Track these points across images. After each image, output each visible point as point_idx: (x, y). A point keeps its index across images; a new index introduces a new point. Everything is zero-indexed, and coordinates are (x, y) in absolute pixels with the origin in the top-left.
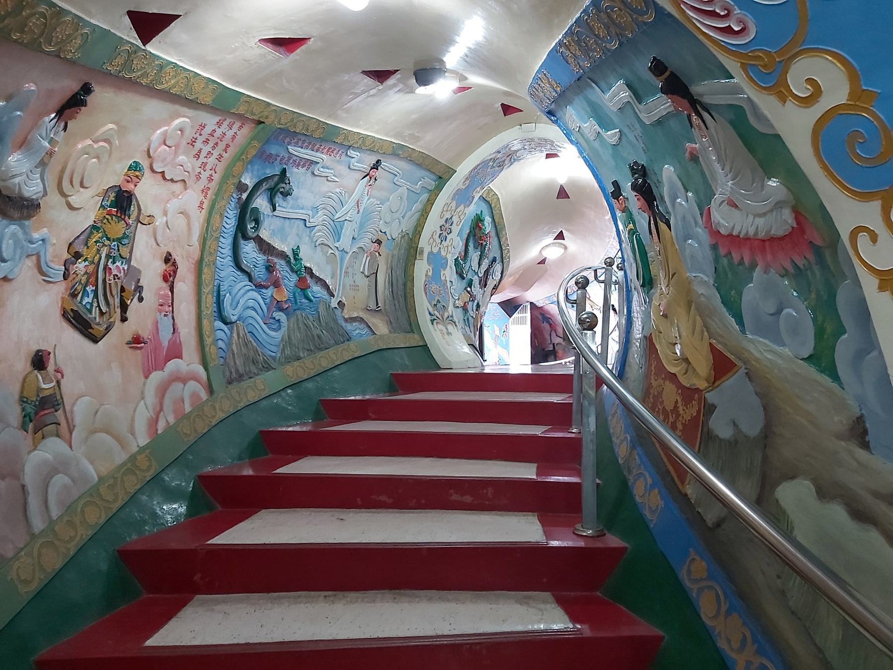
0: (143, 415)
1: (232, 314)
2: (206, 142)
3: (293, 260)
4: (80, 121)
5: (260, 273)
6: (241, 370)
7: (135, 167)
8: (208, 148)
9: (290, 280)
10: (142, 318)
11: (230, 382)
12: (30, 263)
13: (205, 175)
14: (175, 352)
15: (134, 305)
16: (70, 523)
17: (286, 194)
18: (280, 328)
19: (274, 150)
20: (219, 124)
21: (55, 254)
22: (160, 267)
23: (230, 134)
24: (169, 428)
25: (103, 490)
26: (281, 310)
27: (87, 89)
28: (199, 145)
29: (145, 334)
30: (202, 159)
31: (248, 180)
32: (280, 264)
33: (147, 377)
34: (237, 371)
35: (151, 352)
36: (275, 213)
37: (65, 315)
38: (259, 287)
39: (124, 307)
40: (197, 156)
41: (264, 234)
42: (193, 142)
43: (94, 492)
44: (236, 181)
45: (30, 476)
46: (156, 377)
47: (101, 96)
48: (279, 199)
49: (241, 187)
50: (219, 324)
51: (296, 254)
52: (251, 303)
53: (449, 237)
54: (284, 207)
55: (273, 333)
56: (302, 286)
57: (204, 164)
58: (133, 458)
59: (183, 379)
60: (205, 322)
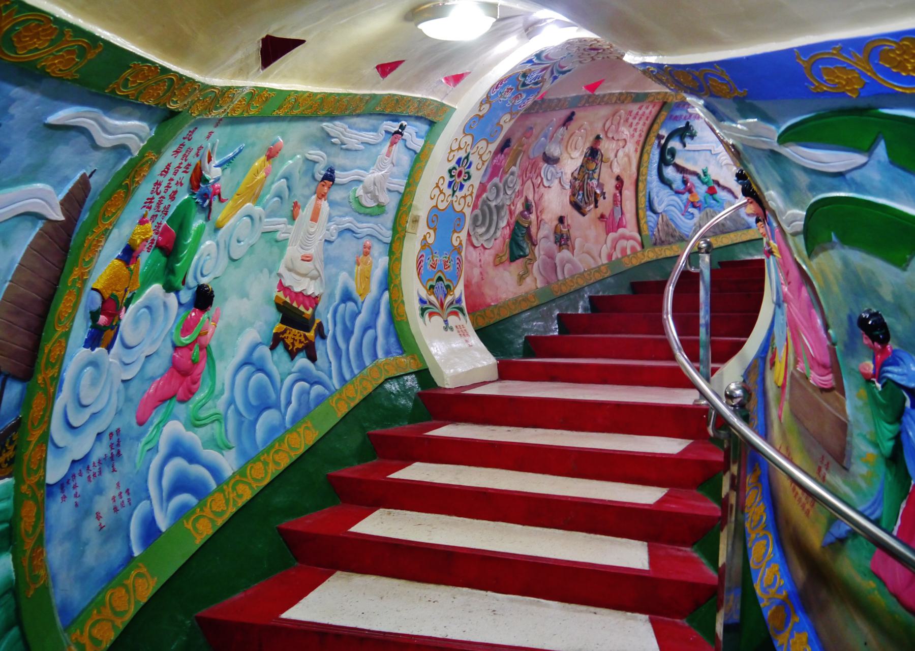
0: (605, 250)
1: (659, 209)
2: (635, 118)
3: (702, 177)
4: (573, 125)
5: (678, 184)
6: (663, 239)
7: (598, 138)
8: (637, 121)
9: (701, 190)
10: (605, 205)
11: (655, 244)
12: (557, 181)
13: (637, 134)
14: (620, 225)
15: (601, 199)
16: (572, 281)
17: (692, 136)
18: (693, 217)
19: (678, 113)
20: (640, 108)
21: (567, 178)
22: (613, 182)
23: (647, 111)
24: (617, 258)
25: (586, 274)
26: (694, 206)
27: (573, 114)
28: (630, 120)
29: (607, 214)
30: (634, 127)
31: (664, 133)
32: (693, 179)
33: (607, 234)
34: (660, 239)
35: (611, 223)
36: (686, 148)
37: (571, 202)
38: (677, 193)
39: (596, 201)
40: (631, 126)
41: (678, 161)
42: (627, 120)
43: (582, 275)
44: (656, 134)
45: (557, 261)
46: (612, 235)
47: (579, 114)
48: (687, 140)
49: (660, 137)
50: (649, 213)
51: (705, 173)
52: (672, 203)
53: (467, 184)
54: (691, 145)
55: (688, 221)
56: (712, 191)
57: (635, 130)
58: (599, 267)
59: (623, 237)
60: (640, 211)
